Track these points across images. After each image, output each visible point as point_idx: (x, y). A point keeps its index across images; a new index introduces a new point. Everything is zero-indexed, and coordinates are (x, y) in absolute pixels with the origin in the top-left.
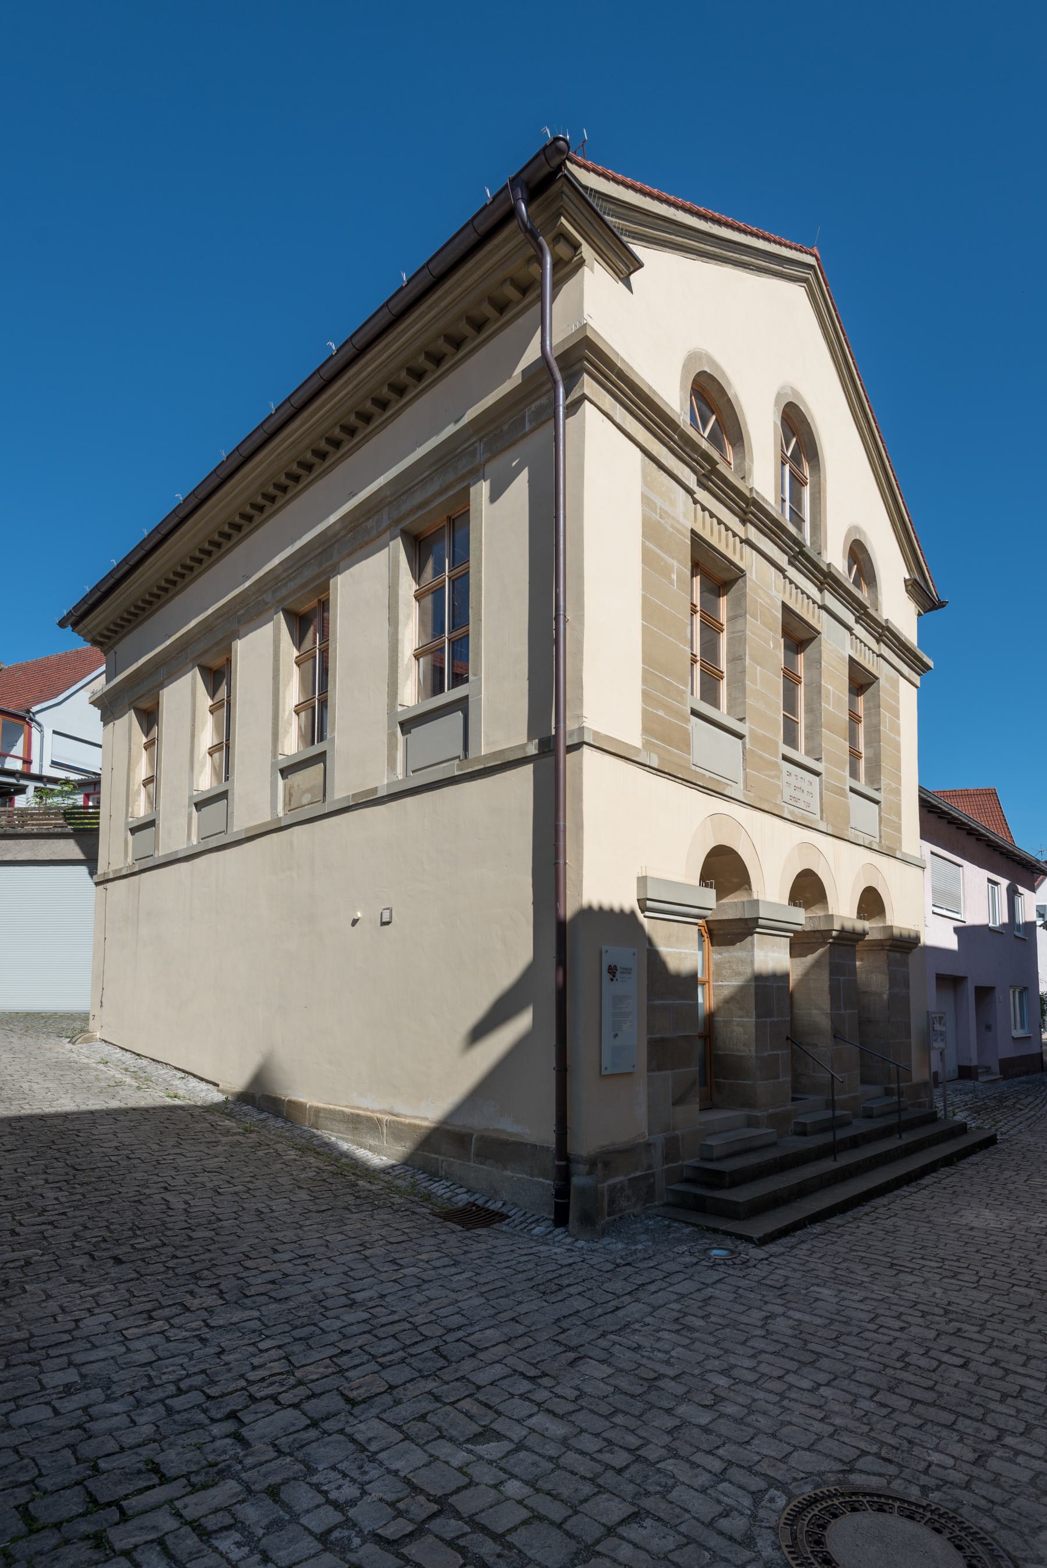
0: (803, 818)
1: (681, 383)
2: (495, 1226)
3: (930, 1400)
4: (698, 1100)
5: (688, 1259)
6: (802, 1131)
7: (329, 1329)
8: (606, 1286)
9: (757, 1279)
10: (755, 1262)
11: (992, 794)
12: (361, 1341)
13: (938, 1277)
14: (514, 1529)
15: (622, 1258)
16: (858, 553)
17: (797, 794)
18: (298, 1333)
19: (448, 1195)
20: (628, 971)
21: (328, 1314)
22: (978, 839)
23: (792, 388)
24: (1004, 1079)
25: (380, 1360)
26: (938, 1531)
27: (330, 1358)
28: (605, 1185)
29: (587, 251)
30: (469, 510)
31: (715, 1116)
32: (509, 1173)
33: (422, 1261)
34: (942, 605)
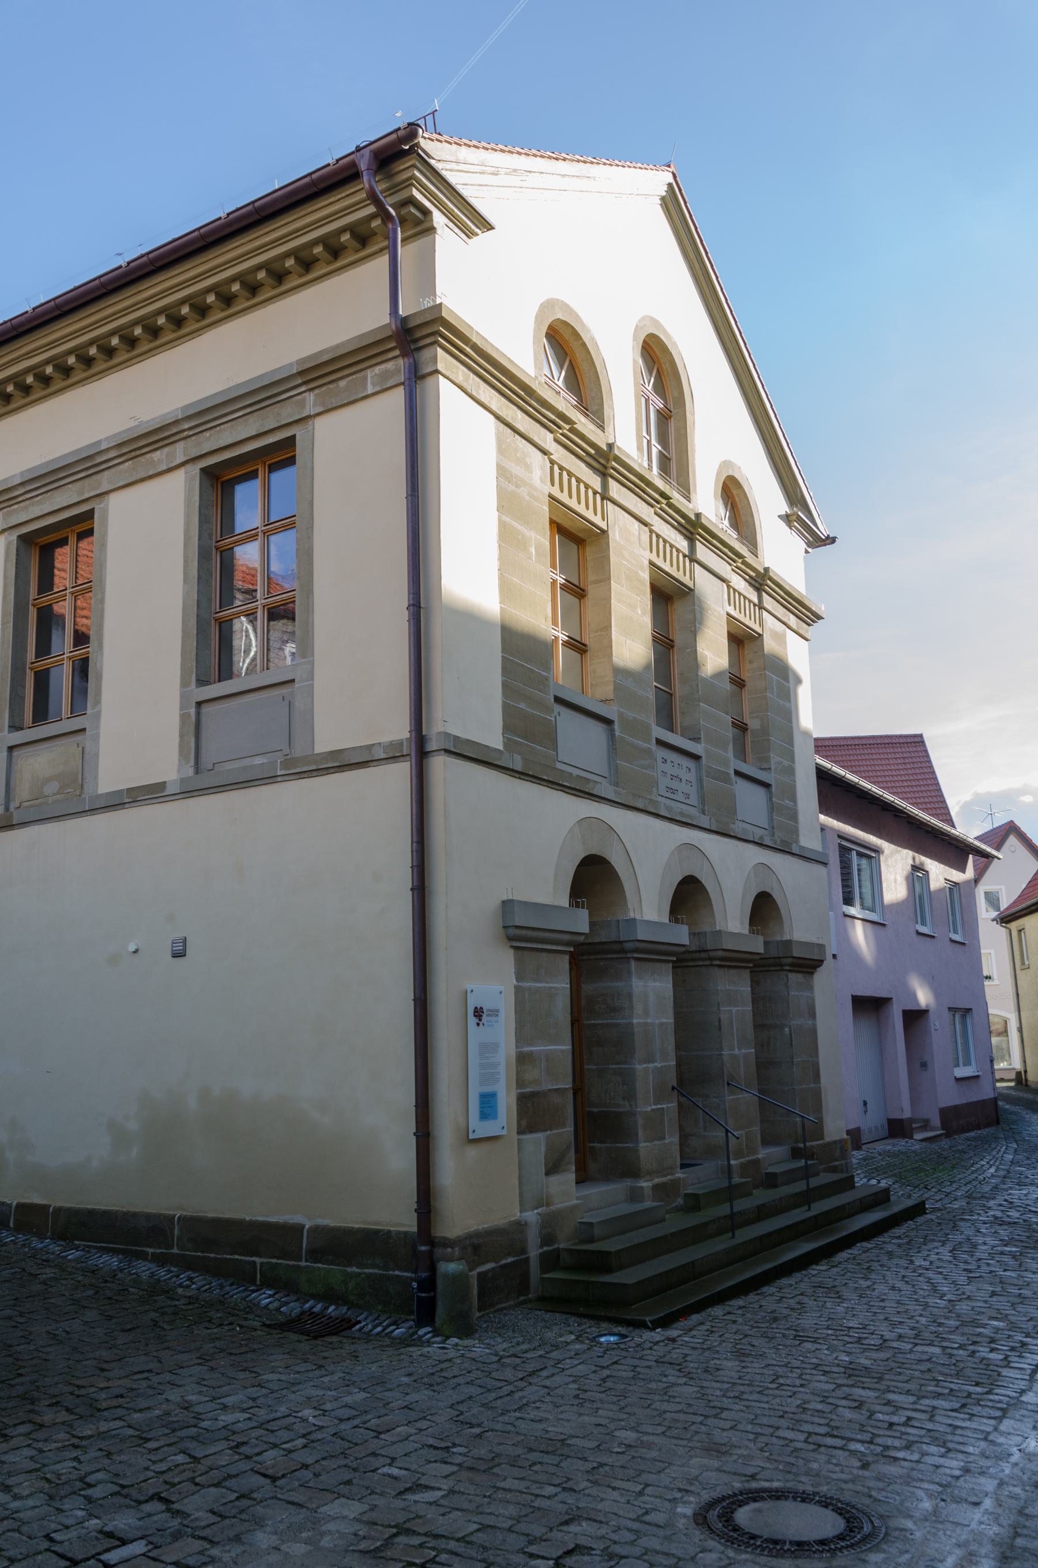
0: (682, 814)
1: (534, 336)
2: (344, 1333)
4: (574, 1168)
6: (694, 1203)
8: (494, 1375)
9: (654, 1358)
11: (917, 742)
13: (840, 1343)
14: (472, 1533)
15: (504, 1350)
16: (731, 491)
17: (674, 784)
19: (276, 1304)
20: (495, 1013)
23: (652, 318)
24: (948, 1135)
26: (826, 1507)
28: (475, 1273)
29: (438, 219)
31: (595, 1192)
32: (355, 1269)
34: (831, 540)
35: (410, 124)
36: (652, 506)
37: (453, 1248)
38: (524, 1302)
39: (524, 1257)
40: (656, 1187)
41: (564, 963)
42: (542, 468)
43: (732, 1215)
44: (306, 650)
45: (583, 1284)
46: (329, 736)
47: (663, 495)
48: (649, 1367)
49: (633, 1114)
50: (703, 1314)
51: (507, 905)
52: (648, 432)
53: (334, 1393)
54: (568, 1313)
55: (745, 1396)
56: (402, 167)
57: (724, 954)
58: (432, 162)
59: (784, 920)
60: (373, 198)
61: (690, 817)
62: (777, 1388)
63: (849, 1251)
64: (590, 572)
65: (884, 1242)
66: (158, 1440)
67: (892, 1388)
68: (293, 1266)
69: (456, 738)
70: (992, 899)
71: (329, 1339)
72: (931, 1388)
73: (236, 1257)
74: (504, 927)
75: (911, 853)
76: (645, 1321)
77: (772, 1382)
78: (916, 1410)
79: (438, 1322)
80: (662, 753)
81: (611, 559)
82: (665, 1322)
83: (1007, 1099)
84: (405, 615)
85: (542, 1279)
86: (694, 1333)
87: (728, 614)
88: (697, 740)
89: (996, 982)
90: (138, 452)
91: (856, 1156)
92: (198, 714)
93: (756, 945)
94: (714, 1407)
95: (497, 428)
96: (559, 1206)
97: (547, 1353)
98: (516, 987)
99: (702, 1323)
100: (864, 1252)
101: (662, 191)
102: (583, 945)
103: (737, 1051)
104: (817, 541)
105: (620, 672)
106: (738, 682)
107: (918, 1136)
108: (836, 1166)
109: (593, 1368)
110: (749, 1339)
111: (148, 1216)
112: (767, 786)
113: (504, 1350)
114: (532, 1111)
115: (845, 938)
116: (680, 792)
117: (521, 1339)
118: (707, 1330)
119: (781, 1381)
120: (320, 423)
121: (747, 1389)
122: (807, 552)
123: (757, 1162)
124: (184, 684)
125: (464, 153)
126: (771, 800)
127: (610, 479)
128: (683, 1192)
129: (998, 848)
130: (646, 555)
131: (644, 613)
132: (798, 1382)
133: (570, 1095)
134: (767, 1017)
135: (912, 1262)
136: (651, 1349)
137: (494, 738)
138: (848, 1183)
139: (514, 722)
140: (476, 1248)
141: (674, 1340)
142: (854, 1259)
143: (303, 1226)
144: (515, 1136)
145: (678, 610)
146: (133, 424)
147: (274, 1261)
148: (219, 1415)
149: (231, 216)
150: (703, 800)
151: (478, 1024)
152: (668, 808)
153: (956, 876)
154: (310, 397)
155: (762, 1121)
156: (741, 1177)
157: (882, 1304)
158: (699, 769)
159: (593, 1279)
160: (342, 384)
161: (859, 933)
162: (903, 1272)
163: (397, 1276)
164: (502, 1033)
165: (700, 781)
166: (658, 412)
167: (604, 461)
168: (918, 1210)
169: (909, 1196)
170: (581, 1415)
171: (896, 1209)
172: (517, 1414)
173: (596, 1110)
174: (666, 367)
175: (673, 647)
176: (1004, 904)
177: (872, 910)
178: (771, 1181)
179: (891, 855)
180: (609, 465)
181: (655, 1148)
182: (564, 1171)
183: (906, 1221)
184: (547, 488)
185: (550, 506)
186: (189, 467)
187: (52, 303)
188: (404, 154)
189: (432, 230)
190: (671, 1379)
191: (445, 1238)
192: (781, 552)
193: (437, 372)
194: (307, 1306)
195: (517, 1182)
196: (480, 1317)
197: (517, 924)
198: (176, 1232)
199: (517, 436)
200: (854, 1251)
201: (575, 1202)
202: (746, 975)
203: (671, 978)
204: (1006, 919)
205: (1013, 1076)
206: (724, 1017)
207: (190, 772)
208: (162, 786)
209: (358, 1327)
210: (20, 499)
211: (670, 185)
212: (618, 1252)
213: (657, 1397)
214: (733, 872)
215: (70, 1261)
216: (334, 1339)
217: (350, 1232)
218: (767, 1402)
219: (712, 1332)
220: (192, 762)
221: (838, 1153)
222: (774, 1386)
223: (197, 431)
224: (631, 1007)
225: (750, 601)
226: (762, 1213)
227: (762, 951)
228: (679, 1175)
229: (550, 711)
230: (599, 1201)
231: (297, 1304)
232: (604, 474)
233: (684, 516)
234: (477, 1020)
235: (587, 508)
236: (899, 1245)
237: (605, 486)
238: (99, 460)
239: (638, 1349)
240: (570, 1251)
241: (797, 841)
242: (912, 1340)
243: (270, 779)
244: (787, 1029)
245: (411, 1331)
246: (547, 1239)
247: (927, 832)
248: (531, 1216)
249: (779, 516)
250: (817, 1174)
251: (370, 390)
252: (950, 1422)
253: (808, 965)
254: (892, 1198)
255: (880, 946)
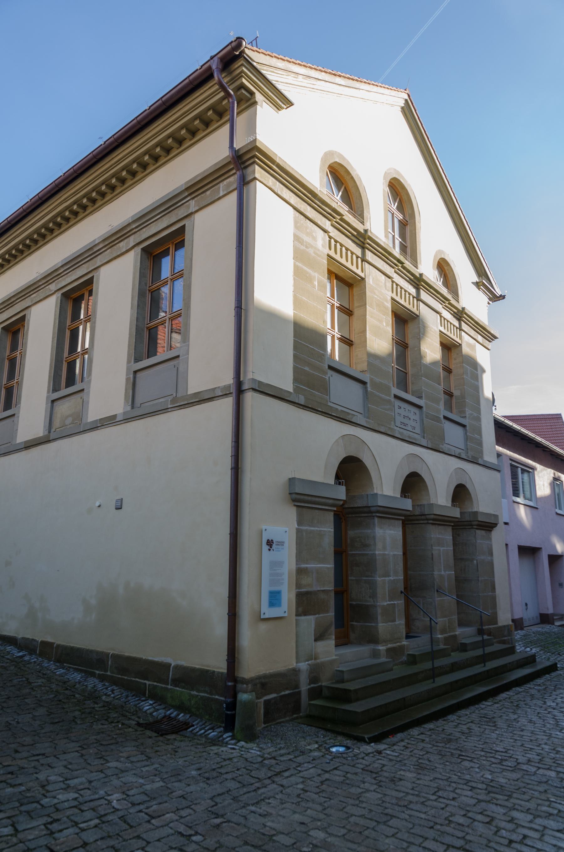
0: (409, 437)
2: (181, 733)
3: (458, 846)
4: (334, 637)
5: (316, 754)
6: (413, 660)
7: (47, 805)
8: (253, 774)
9: (362, 766)
10: (363, 755)
12: (69, 812)
13: (489, 763)
15: (269, 754)
16: (443, 267)
18: (23, 808)
19: (151, 710)
20: (281, 543)
21: (48, 795)
22: (544, 450)
23: (395, 169)
25: (81, 825)
27: (45, 825)
28: (262, 700)
29: (259, 97)
30: (184, 240)
31: (348, 651)
32: (195, 693)
33: (123, 757)
34: (503, 297)
35: (238, 38)
36: (393, 268)
37: (247, 685)
38: (297, 718)
39: (297, 690)
40: (388, 650)
42: (323, 239)
43: (433, 669)
44: (186, 340)
45: (334, 710)
46: (196, 384)
47: (399, 261)
48: (356, 774)
49: (375, 606)
50: (405, 733)
51: (292, 481)
52: (393, 231)
53: (141, 781)
54: (320, 728)
55: (411, 806)
56: (236, 66)
57: (435, 517)
58: (255, 64)
59: (474, 500)
61: (415, 439)
62: (436, 800)
63: (508, 693)
64: (355, 302)
65: (530, 688)
66: (5, 812)
67: (516, 807)
68: (165, 688)
69: (259, 382)
71: (169, 737)
72: (544, 808)
73: (137, 679)
74: (290, 494)
75: (552, 471)
76: (364, 738)
77: (433, 794)
78: (531, 829)
79: (235, 731)
80: (398, 403)
81: (367, 294)
82: (377, 739)
85: (310, 704)
86: (395, 747)
87: (440, 331)
88: (420, 397)
90: (113, 244)
91: (518, 635)
92: (135, 378)
94: (386, 814)
95: (295, 218)
96: (322, 660)
97: (295, 757)
98: (297, 529)
99: (402, 740)
100: (517, 694)
101: (402, 103)
102: (343, 507)
103: (443, 571)
104: (495, 298)
105: (372, 356)
106: (448, 370)
107: (557, 623)
108: (505, 640)
109: (320, 772)
110: (428, 755)
111: (97, 653)
112: (464, 426)
113: (269, 754)
114: (306, 603)
116: (409, 425)
117: (282, 746)
118: (404, 746)
119: (440, 793)
120: (197, 216)
121: (415, 799)
122: (489, 303)
123: (455, 637)
124: (129, 362)
125: (274, 62)
126: (466, 434)
127: (367, 250)
128: (406, 653)
130: (389, 294)
131: (387, 325)
132: (452, 795)
133: (332, 594)
134: (461, 555)
135: (545, 703)
136: (363, 758)
137: (286, 383)
138: (511, 651)
139: (299, 376)
140: (263, 685)
141: (380, 753)
142: (510, 698)
143: (171, 665)
144: (294, 618)
145: (411, 328)
146: (110, 228)
147: (155, 684)
148: (59, 794)
149: (152, 108)
150: (423, 430)
151: (269, 550)
152: (401, 434)
154: (192, 203)
155: (458, 613)
156: (444, 645)
157: (522, 733)
158: (421, 414)
159: (337, 707)
160: (208, 193)
161: (522, 512)
162: (538, 710)
163: (217, 699)
164: (287, 557)
165: (422, 421)
167: (363, 240)
168: (553, 668)
169: (549, 659)
170: (295, 812)
171: (539, 667)
172: (253, 808)
173: (354, 603)
174: (404, 197)
175: (407, 347)
177: (530, 500)
178: (463, 648)
179: (542, 471)
180: (365, 242)
181: (389, 626)
182: (327, 639)
183: (545, 674)
184: (326, 251)
186: (136, 248)
187: (72, 170)
188: (236, 58)
189: (255, 103)
190: (367, 785)
191: (243, 678)
192: (473, 301)
193: (255, 179)
194: (169, 712)
195: (294, 645)
196: (264, 728)
198: (110, 663)
199: (307, 221)
200: (510, 693)
201: (334, 657)
202: (450, 530)
203: (401, 529)
206: (435, 553)
207: (129, 408)
208: (115, 416)
209: (191, 729)
210: (62, 275)
211: (406, 100)
212: (356, 691)
213: (351, 801)
214: (441, 473)
215: (56, 675)
216: (173, 736)
217: (193, 670)
218: (425, 813)
219: (407, 748)
220: (130, 403)
221: (506, 633)
222: (434, 797)
223: (140, 228)
224: (375, 544)
225: (454, 326)
226: (454, 667)
228: (405, 643)
230: (354, 656)
231: (163, 711)
232: (363, 247)
233: (412, 274)
234: (268, 547)
235: (352, 264)
236: (539, 691)
237: (364, 254)
238: (95, 250)
239: (354, 758)
240: (328, 688)
241: (482, 457)
242: (537, 765)
243: (165, 410)
244: (475, 562)
245: (220, 734)
246: (314, 679)
248: (304, 666)
249: (473, 283)
250: (493, 644)
251: (221, 194)
252: (554, 842)
253: (489, 526)
254: (538, 660)
255: (534, 519)
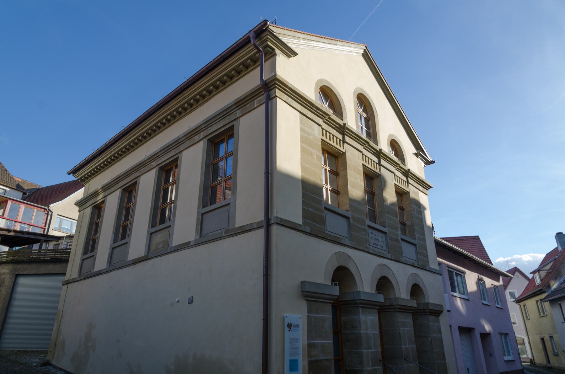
0: (379, 253)
11: (477, 238)
16: (394, 145)
20: (297, 326)
29: (277, 51)
34: (433, 162)
41: (330, 307)
46: (240, 221)
47: (366, 141)
51: (303, 283)
52: (361, 124)
60: (256, 47)
70: (512, 295)
80: (370, 231)
83: (526, 369)
84: (263, 176)
88: (385, 227)
89: (517, 325)
93: (414, 304)
102: (337, 301)
103: (408, 346)
105: (353, 201)
106: (402, 209)
112: (415, 245)
115: (453, 305)
120: (241, 119)
124: (199, 208)
125: (286, 32)
129: (513, 274)
130: (361, 162)
133: (333, 362)
134: (420, 333)
137: (299, 220)
145: (376, 182)
152: (373, 250)
153: (496, 283)
154: (239, 112)
160: (248, 105)
164: (301, 335)
165: (387, 242)
166: (365, 118)
176: (517, 296)
177: (464, 294)
184: (321, 137)
185: (322, 142)
186: (204, 139)
188: (264, 31)
189: (276, 54)
192: (414, 165)
193: (276, 96)
197: (307, 290)
202: (410, 315)
204: (518, 301)
205: (529, 361)
207: (198, 237)
211: (365, 50)
214: (402, 276)
223: (207, 127)
227: (416, 306)
229: (323, 212)
237: (344, 138)
241: (428, 266)
243: (221, 238)
247: (482, 267)
255: (467, 307)
